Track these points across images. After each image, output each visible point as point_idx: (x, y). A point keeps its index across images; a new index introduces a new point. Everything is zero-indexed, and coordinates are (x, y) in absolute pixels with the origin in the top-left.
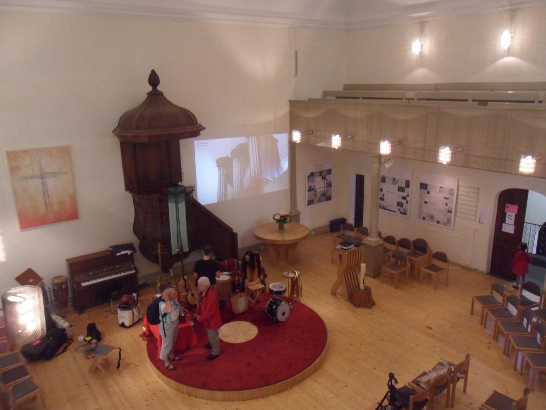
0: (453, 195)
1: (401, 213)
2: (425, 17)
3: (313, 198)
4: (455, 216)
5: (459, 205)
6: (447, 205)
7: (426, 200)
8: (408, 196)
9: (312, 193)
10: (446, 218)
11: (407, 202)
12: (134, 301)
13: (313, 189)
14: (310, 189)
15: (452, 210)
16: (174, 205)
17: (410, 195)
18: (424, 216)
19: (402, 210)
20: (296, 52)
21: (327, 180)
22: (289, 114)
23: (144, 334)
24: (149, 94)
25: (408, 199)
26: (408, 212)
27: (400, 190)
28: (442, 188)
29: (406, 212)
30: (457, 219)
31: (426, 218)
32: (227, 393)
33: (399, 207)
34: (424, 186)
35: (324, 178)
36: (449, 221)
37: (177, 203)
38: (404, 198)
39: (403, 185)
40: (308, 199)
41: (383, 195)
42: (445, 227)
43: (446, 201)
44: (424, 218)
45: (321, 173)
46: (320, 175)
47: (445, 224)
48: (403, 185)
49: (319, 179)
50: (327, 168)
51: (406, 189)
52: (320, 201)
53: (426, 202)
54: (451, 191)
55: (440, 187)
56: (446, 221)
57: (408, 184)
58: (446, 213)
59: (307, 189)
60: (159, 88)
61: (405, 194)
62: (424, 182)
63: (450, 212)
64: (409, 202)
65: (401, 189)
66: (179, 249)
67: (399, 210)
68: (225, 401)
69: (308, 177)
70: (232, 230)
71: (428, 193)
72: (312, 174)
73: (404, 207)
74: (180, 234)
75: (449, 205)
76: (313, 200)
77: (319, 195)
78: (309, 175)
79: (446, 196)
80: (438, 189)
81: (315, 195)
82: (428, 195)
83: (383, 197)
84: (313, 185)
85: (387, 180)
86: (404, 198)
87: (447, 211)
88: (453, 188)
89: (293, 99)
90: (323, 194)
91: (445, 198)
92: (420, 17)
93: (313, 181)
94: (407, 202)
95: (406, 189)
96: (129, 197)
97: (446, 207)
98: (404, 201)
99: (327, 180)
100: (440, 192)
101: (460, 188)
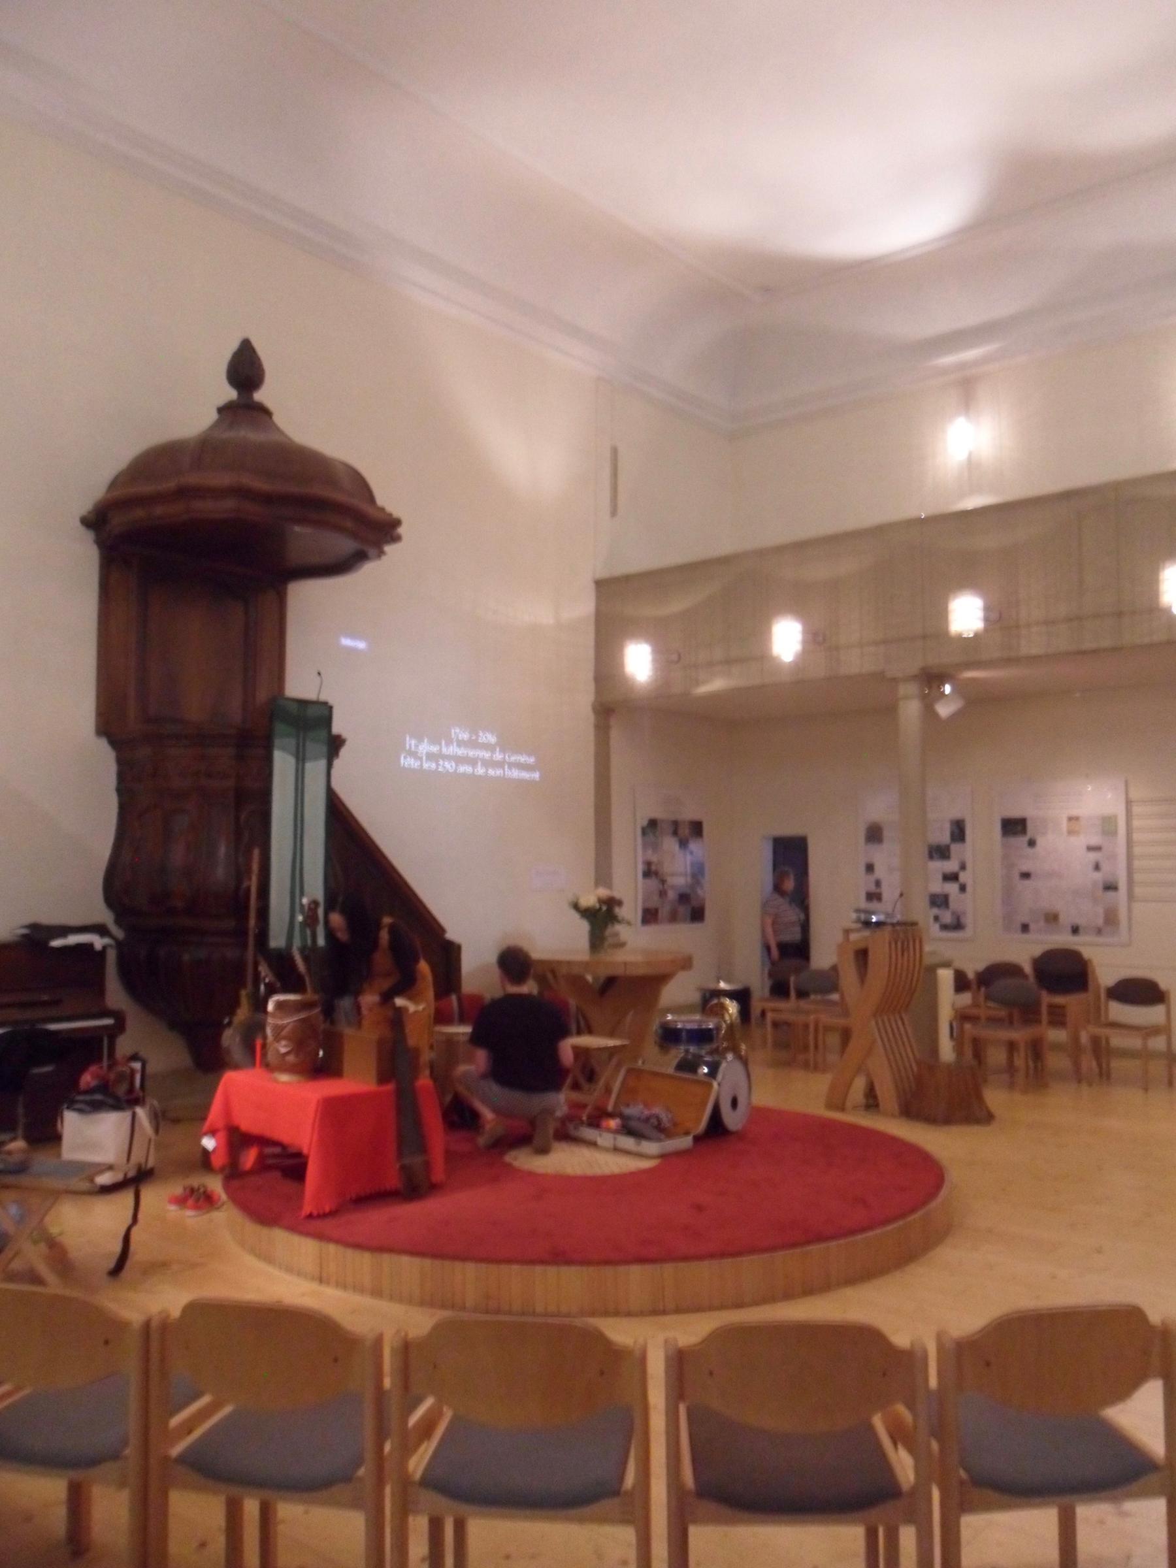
0: (1115, 833)
1: (945, 927)
2: (976, 363)
3: (655, 902)
4: (1131, 896)
5: (1137, 864)
6: (1097, 867)
7: (1025, 868)
8: (963, 867)
9: (653, 883)
10: (1100, 910)
11: (963, 888)
12: (131, 1090)
13: (656, 874)
14: (649, 872)
15: (1117, 883)
16: (291, 761)
17: (969, 866)
18: (1025, 919)
19: (947, 918)
20: (615, 451)
21: (691, 853)
22: (593, 619)
23: (188, 1190)
24: (226, 410)
25: (963, 877)
26: (968, 920)
27: (935, 855)
28: (1077, 819)
29: (963, 920)
30: (1138, 907)
31: (1032, 926)
32: (668, 1270)
33: (935, 911)
34: (1014, 827)
35: (683, 844)
36: (1111, 919)
37: (301, 758)
38: (951, 877)
39: (944, 837)
40: (644, 901)
41: (878, 883)
42: (1101, 940)
43: (1093, 856)
44: (1025, 928)
45: (675, 827)
46: (675, 833)
47: (1099, 931)
48: (944, 837)
49: (670, 844)
50: (689, 813)
51: (955, 848)
52: (673, 918)
53: (1026, 875)
54: (1107, 825)
55: (1070, 819)
56: (1100, 921)
57: (959, 831)
58: (1100, 892)
59: (640, 868)
60: (259, 396)
61: (951, 866)
62: (1015, 813)
63: (1110, 887)
64: (969, 889)
65: (940, 852)
66: (304, 917)
67: (936, 918)
68: (664, 1312)
69: (644, 832)
70: (443, 931)
71: (1032, 843)
72: (653, 823)
73: (953, 904)
74: (301, 869)
75: (1105, 867)
76: (656, 911)
77: (672, 895)
78: (645, 823)
79: (1095, 840)
80: (1064, 824)
81: (662, 894)
82: (1030, 851)
83: (878, 891)
84: (654, 859)
85: (886, 834)
86: (951, 877)
87: (1101, 886)
88: (1108, 810)
89: (603, 574)
90: (684, 898)
91: (1090, 849)
92: (962, 366)
93: (655, 847)
94: (963, 888)
95: (955, 848)
96: (104, 759)
97: (1098, 876)
98: (952, 888)
99: (691, 853)
100: (1071, 832)
101: (1136, 809)
